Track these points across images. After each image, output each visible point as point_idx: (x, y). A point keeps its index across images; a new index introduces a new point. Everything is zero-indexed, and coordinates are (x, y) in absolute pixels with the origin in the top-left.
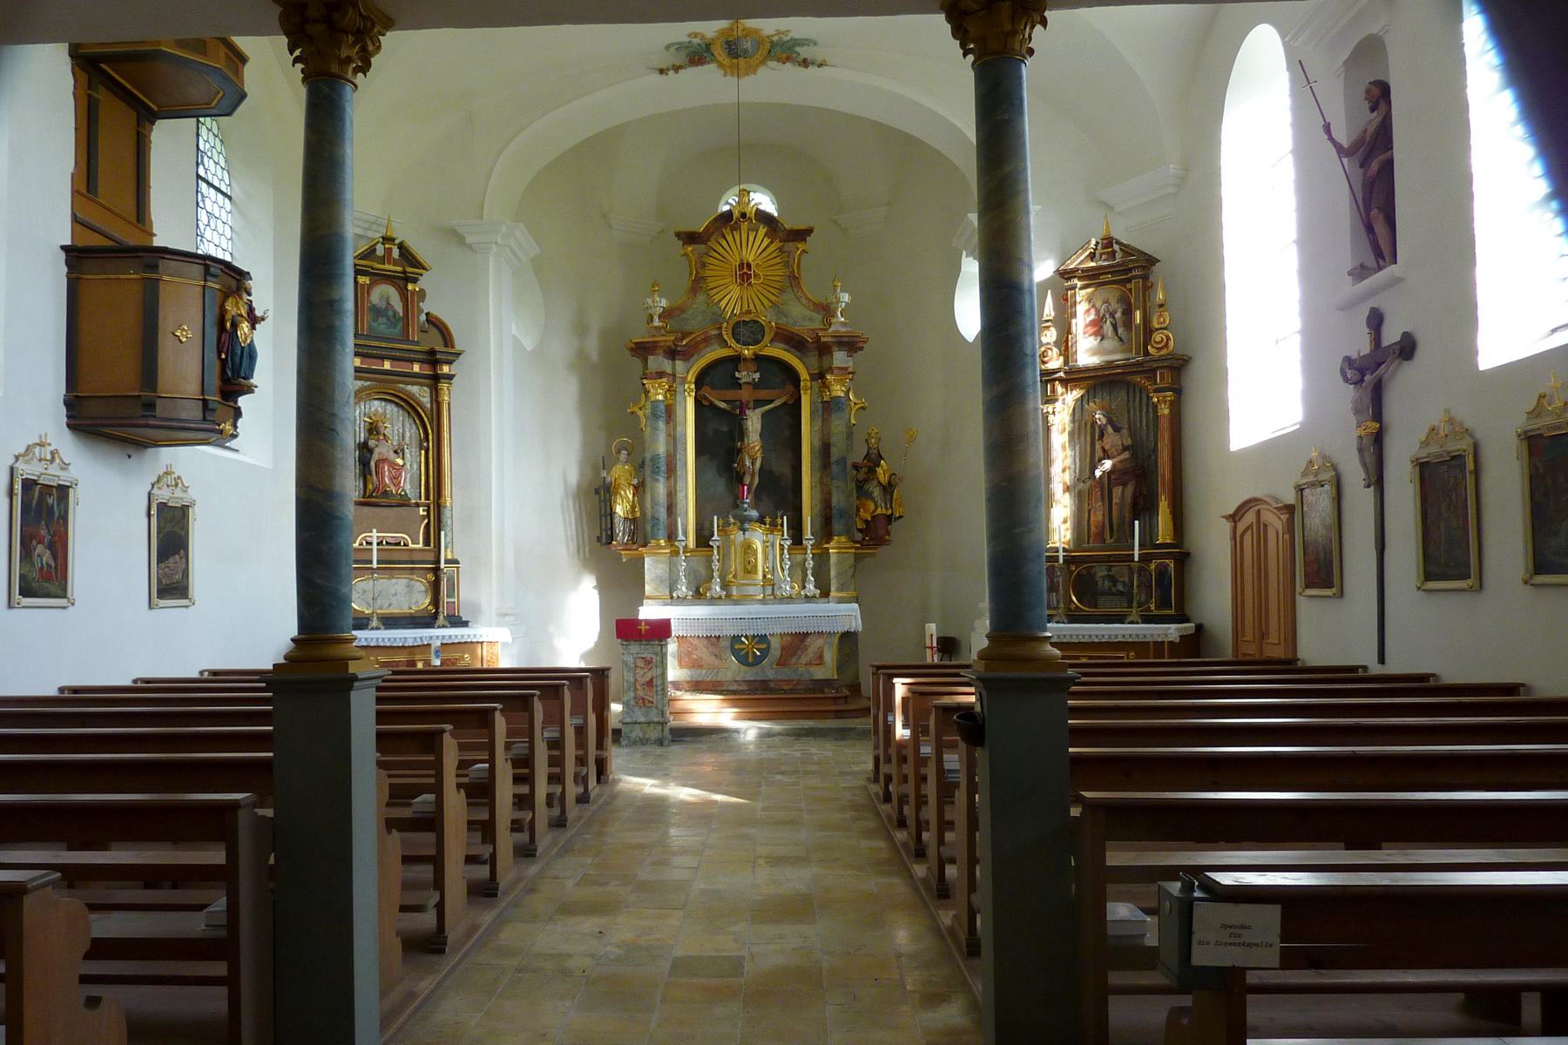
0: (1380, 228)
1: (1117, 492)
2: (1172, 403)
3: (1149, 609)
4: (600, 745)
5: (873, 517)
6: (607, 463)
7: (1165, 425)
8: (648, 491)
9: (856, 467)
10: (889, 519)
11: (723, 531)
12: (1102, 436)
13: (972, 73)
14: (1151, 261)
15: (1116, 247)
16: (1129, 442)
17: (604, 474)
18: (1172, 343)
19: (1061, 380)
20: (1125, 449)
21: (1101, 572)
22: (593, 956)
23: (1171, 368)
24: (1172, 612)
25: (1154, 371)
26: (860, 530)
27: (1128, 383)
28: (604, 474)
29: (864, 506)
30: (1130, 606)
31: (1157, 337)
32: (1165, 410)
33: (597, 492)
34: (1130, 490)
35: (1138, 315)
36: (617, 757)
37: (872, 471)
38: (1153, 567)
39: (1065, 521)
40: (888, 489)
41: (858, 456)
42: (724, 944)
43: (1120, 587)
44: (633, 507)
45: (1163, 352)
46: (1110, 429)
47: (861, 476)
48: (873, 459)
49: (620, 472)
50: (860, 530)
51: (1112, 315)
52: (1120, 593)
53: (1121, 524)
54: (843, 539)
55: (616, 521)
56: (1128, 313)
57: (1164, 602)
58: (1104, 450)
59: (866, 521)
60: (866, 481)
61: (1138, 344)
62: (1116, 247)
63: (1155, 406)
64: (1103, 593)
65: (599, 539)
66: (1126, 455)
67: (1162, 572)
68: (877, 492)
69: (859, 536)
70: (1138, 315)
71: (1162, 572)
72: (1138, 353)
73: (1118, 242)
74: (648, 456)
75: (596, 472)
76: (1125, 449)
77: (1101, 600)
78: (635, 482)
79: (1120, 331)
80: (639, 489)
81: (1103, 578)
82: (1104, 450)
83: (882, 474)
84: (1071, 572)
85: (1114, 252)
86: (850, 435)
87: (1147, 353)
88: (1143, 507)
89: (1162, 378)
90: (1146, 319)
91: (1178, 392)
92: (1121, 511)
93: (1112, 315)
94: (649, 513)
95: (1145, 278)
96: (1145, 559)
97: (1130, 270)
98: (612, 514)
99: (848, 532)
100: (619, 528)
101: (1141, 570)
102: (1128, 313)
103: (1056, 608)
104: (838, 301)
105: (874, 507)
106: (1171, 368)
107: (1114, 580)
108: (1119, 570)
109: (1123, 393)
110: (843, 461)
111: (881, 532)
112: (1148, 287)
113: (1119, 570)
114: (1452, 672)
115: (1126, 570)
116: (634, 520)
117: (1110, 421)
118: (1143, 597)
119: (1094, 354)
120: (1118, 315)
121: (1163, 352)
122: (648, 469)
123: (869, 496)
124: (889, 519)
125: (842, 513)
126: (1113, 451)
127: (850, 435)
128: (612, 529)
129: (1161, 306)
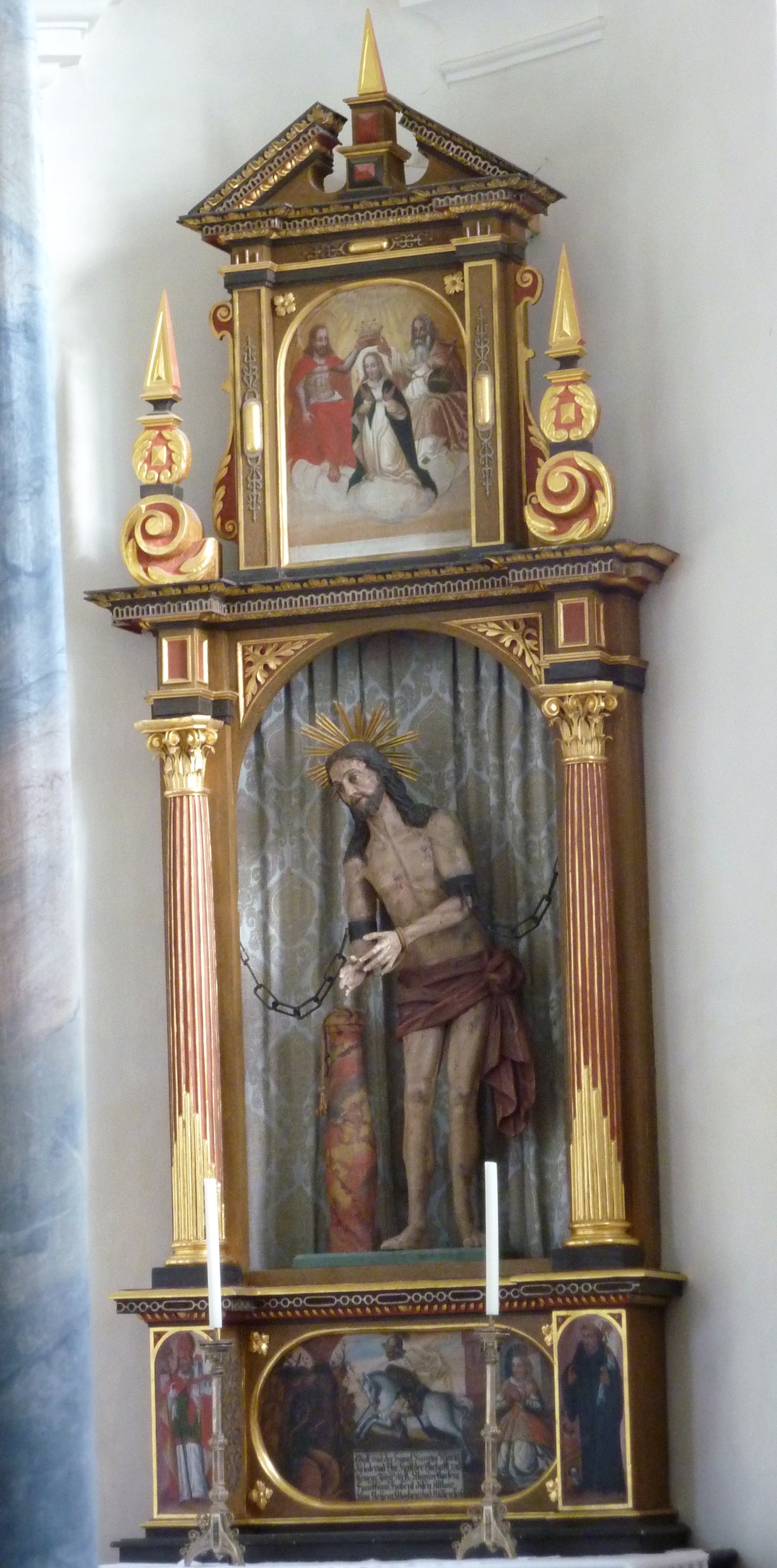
1: (419, 1048)
2: (610, 721)
3: (541, 1500)
4: (243, 401)
7: (585, 806)
12: (362, 838)
14: (532, 197)
15: (406, 138)
16: (456, 863)
18: (604, 506)
19: (211, 628)
20: (449, 888)
21: (363, 1356)
22: (218, 486)
23: (603, 590)
24: (624, 1508)
25: (544, 597)
27: (453, 643)
30: (473, 1490)
31: (554, 476)
32: (584, 747)
34: (465, 1040)
35: (485, 395)
36: (316, 354)
38: (553, 1335)
43: (436, 1416)
45: (579, 531)
46: (389, 815)
51: (394, 389)
52: (436, 1439)
53: (436, 1172)
56: (450, 381)
57: (594, 1473)
58: (371, 892)
61: (486, 498)
62: (406, 138)
63: (552, 733)
64: (373, 1442)
66: (451, 912)
67: (586, 1358)
70: (485, 395)
71: (586, 1358)
72: (486, 531)
73: (414, 120)
76: (449, 888)
77: (368, 1466)
79: (424, 447)
81: (373, 1382)
82: (371, 892)
84: (254, 1362)
85: (397, 158)
87: (518, 534)
88: (515, 1108)
89: (574, 631)
90: (514, 412)
91: (632, 676)
92: (432, 1129)
93: (394, 389)
95: (510, 256)
96: (524, 1305)
97: (454, 226)
101: (511, 1348)
102: (450, 381)
103: (202, 1503)
106: (603, 590)
107: (410, 1388)
108: (435, 1351)
109: (437, 678)
112: (517, 295)
113: (435, 1351)
115: (455, 1351)
117: (391, 785)
118: (521, 1455)
120: (416, 390)
121: (579, 531)
126: (400, 900)
129: (567, 362)
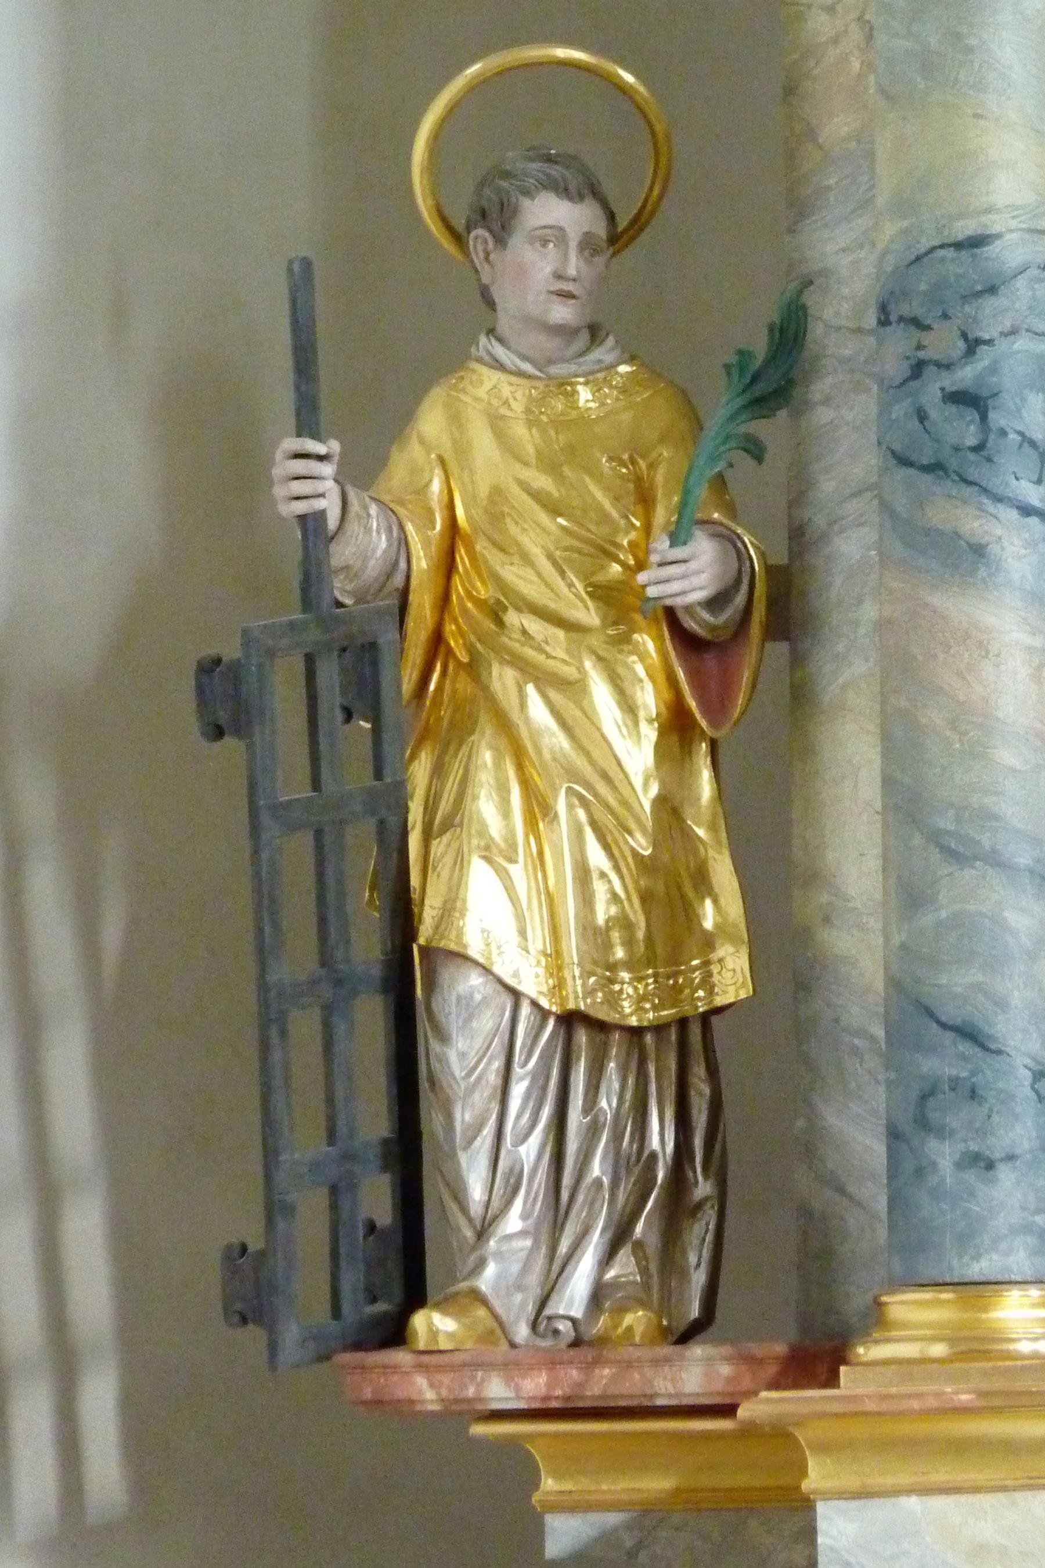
0: (848, 1496)
6: (350, 353)
8: (849, 674)
17: (307, 480)
28: (307, 480)
33: (224, 701)
42: (602, 543)
44: (668, 890)
49: (499, 456)
55: (466, 1049)
65: (250, 1292)
74: (849, 256)
75: (208, 450)
78: (691, 575)
80: (744, 658)
94: (859, 948)
98: (406, 975)
100: (497, 1134)
104: (1009, 1252)
114: (877, 1500)
116: (687, 1046)
122: (847, 421)
128: (408, 1152)
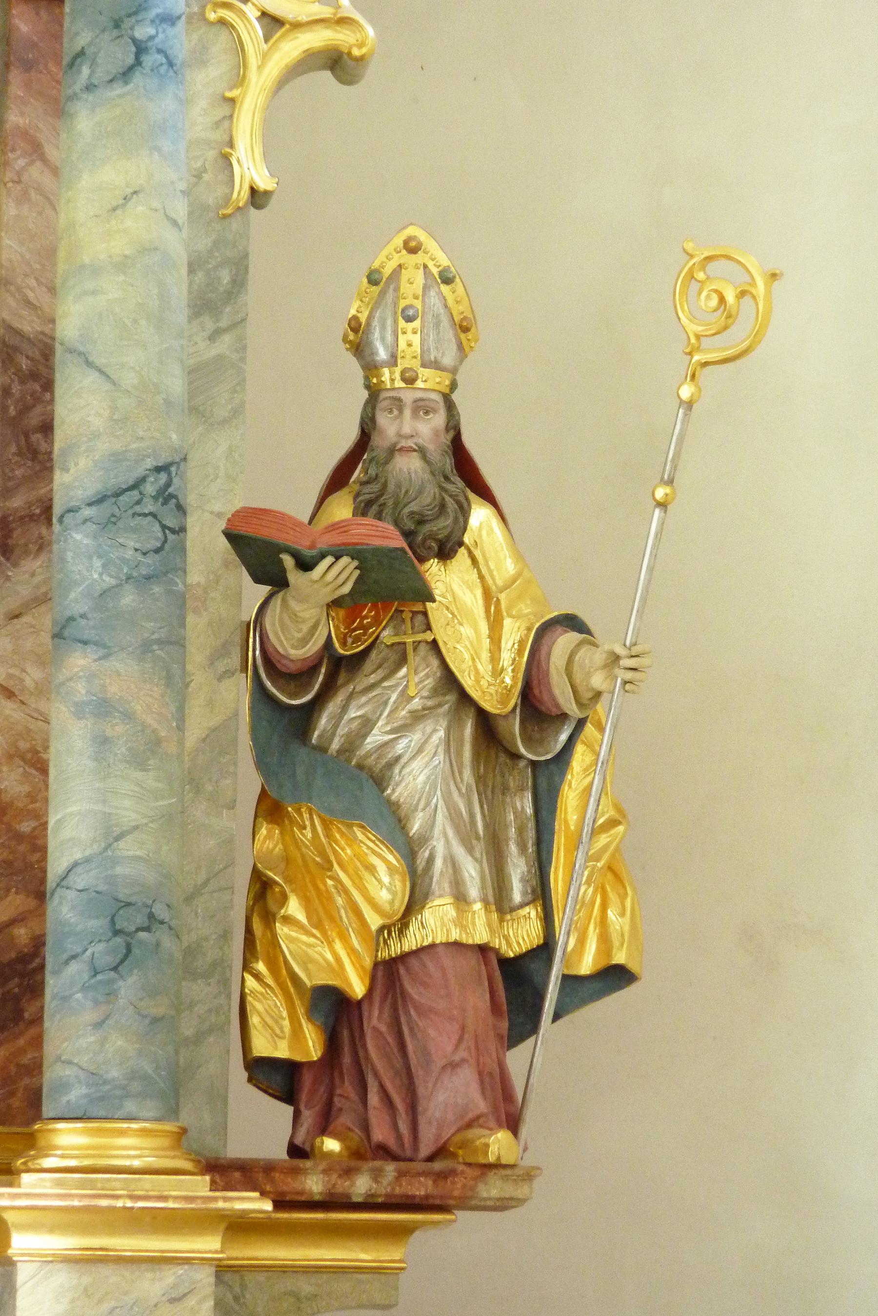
5: (389, 973)
9: (262, 554)
10: (519, 988)
11: (399, 1137)
13: (17, 1305)
26: (279, 1078)
29: (314, 874)
37: (390, 589)
39: (341, 1109)
40: (520, 739)
41: (275, 458)
47: (303, 623)
48: (404, 505)
50: (279, 1078)
54: (133, 1145)
59: (333, 1008)
60: (338, 667)
68: (425, 767)
69: (262, 1127)
83: (478, 622)
86: (219, 290)
99: (169, 1091)
105: (402, 880)
110: (154, 495)
111: (449, 1095)
119: (38, 1131)
123: (365, 790)
124: (519, 988)
125: (133, 927)
127: (219, 290)
